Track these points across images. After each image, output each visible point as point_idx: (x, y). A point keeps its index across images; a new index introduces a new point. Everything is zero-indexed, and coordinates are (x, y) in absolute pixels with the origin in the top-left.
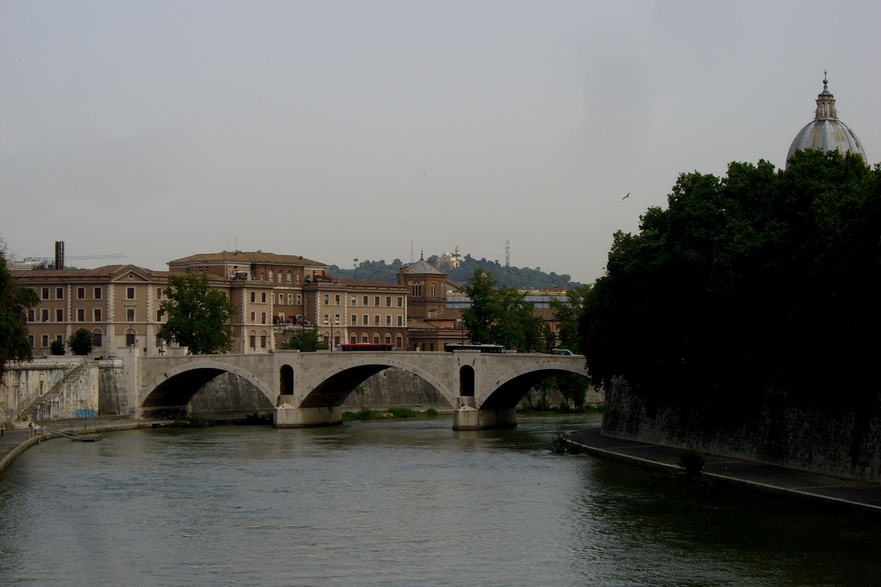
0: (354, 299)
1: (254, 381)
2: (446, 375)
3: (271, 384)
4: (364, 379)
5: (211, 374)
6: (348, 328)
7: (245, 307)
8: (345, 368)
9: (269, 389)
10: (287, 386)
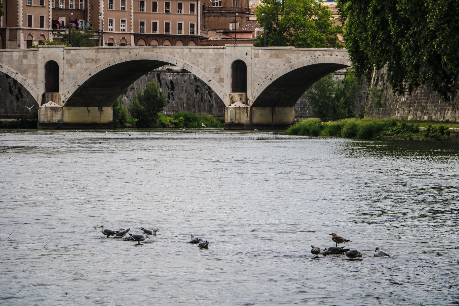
1: (19, 78)
2: (218, 70)
3: (35, 81)
4: (135, 79)
6: (135, 35)
7: (21, 9)
8: (112, 64)
9: (33, 86)
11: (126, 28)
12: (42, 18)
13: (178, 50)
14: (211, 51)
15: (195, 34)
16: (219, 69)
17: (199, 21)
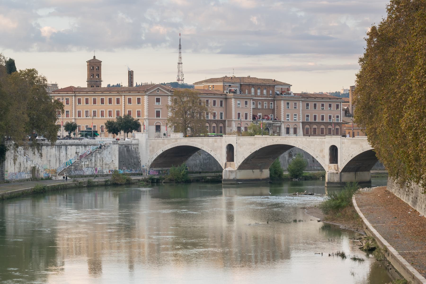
0: (239, 102)
2: (322, 151)
5: (192, 150)
6: (303, 123)
7: (233, 110)
10: (230, 157)
11: (297, 119)
12: (246, 114)
13: (300, 139)
14: (318, 139)
15: (339, 122)
16: (322, 150)
17: (342, 114)
